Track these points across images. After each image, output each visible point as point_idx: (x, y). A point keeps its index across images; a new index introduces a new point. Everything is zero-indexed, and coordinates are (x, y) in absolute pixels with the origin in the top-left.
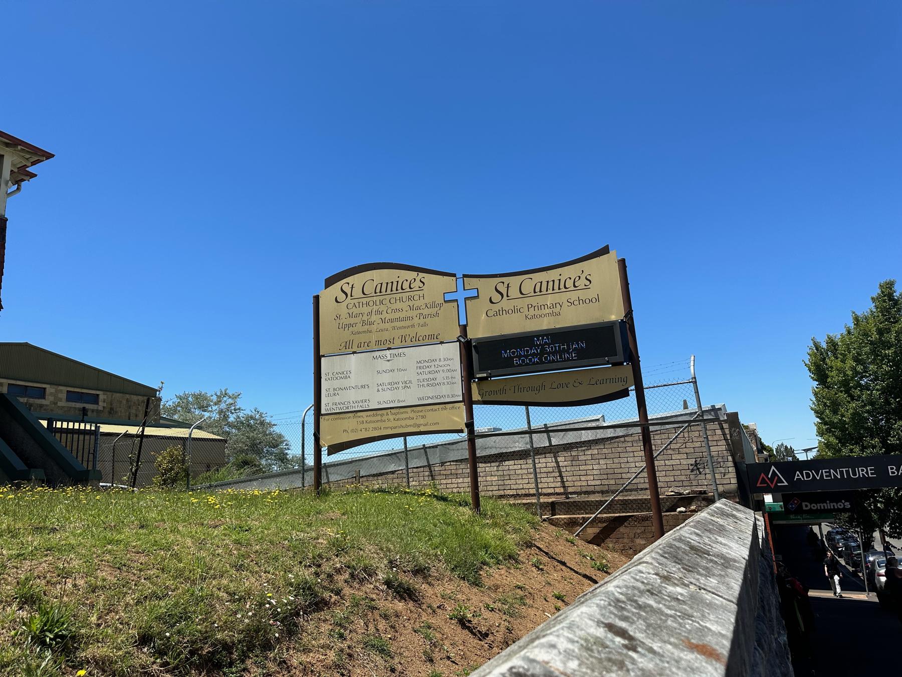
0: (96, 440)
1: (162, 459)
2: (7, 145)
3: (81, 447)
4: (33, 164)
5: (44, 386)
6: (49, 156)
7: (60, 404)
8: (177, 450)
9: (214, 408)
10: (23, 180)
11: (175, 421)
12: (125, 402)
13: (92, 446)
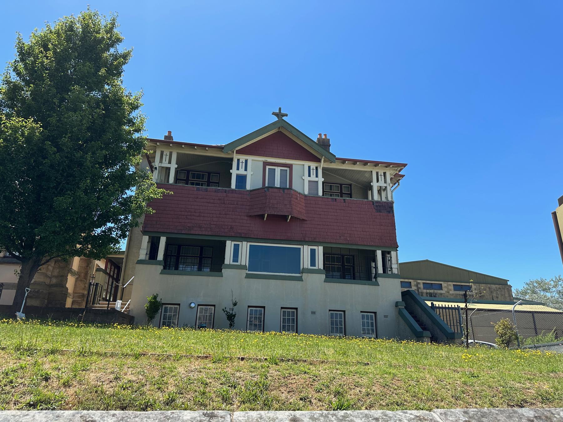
0: (459, 312)
1: (499, 327)
2: (386, 167)
3: (451, 319)
4: (399, 171)
5: (441, 283)
6: (405, 165)
7: (451, 292)
8: (507, 321)
9: (554, 289)
10: (399, 180)
11: (525, 300)
12: (488, 289)
13: (457, 316)
